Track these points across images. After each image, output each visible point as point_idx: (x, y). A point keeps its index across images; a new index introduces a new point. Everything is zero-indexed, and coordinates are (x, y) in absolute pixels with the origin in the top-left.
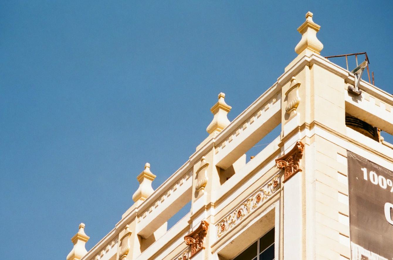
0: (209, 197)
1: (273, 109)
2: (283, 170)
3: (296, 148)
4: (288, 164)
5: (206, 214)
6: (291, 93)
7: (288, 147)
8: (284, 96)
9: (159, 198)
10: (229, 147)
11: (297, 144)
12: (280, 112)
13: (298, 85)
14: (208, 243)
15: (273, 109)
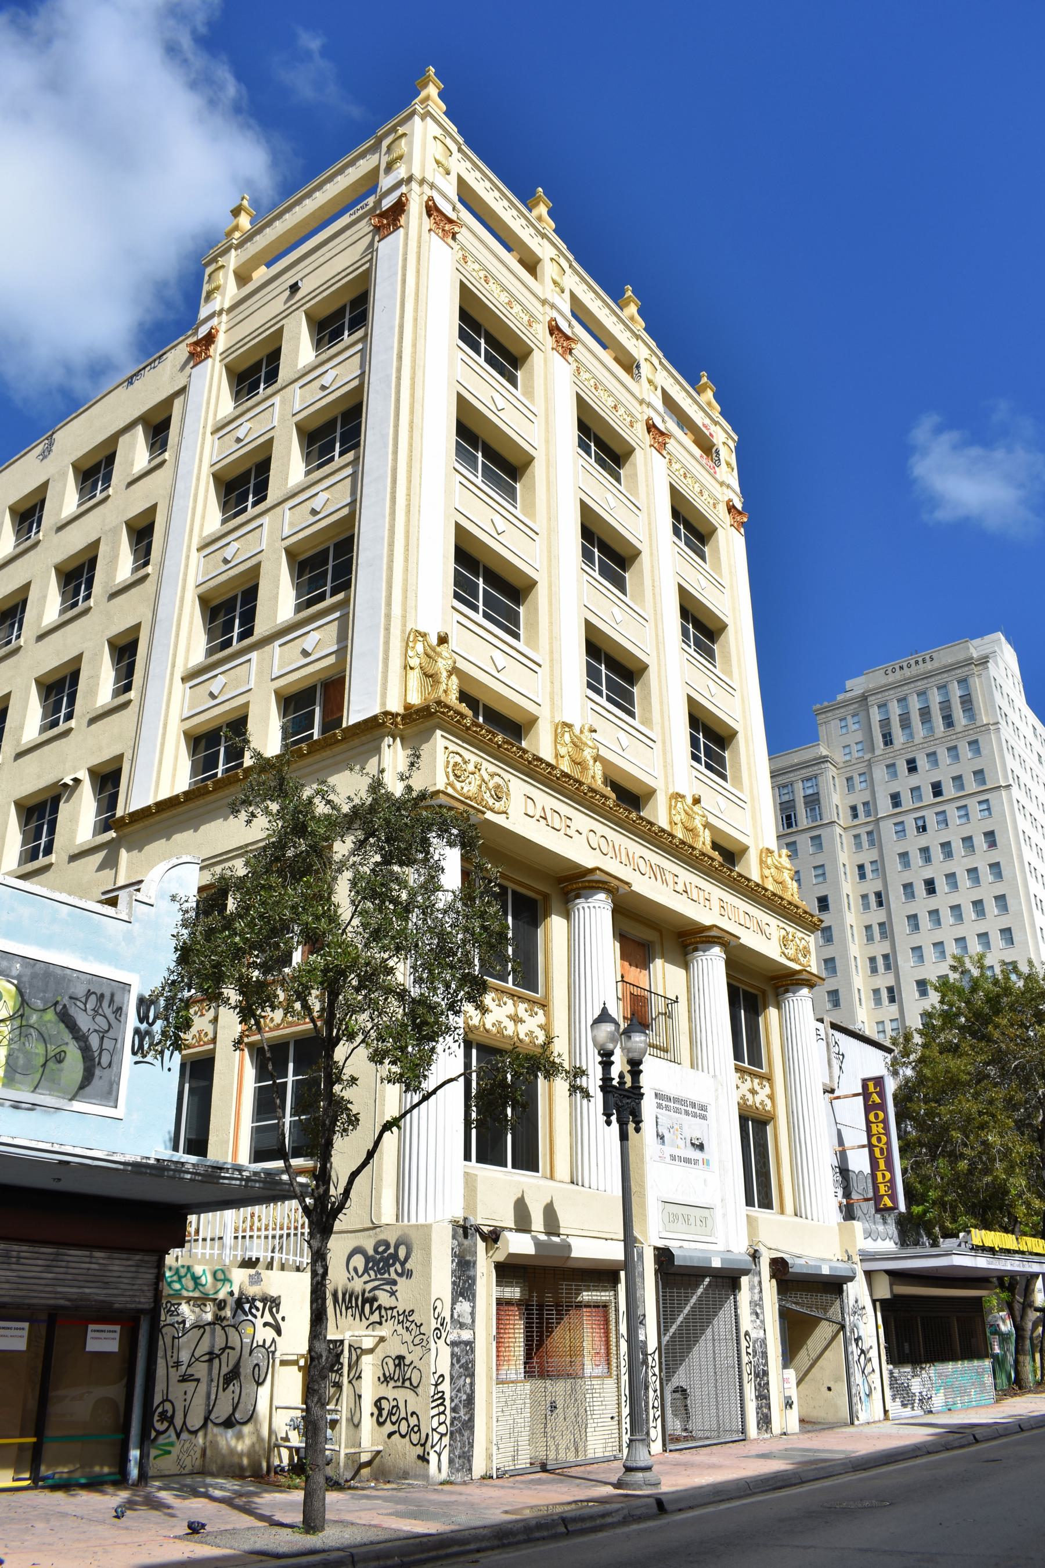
0: (222, 302)
1: (365, 166)
2: (377, 229)
3: (210, 333)
4: (385, 222)
5: (215, 321)
6: (216, 274)
7: (387, 203)
8: (384, 149)
9: (259, 231)
10: (253, 248)
11: (212, 328)
12: (378, 167)
13: (223, 266)
14: (215, 350)
15: (365, 166)
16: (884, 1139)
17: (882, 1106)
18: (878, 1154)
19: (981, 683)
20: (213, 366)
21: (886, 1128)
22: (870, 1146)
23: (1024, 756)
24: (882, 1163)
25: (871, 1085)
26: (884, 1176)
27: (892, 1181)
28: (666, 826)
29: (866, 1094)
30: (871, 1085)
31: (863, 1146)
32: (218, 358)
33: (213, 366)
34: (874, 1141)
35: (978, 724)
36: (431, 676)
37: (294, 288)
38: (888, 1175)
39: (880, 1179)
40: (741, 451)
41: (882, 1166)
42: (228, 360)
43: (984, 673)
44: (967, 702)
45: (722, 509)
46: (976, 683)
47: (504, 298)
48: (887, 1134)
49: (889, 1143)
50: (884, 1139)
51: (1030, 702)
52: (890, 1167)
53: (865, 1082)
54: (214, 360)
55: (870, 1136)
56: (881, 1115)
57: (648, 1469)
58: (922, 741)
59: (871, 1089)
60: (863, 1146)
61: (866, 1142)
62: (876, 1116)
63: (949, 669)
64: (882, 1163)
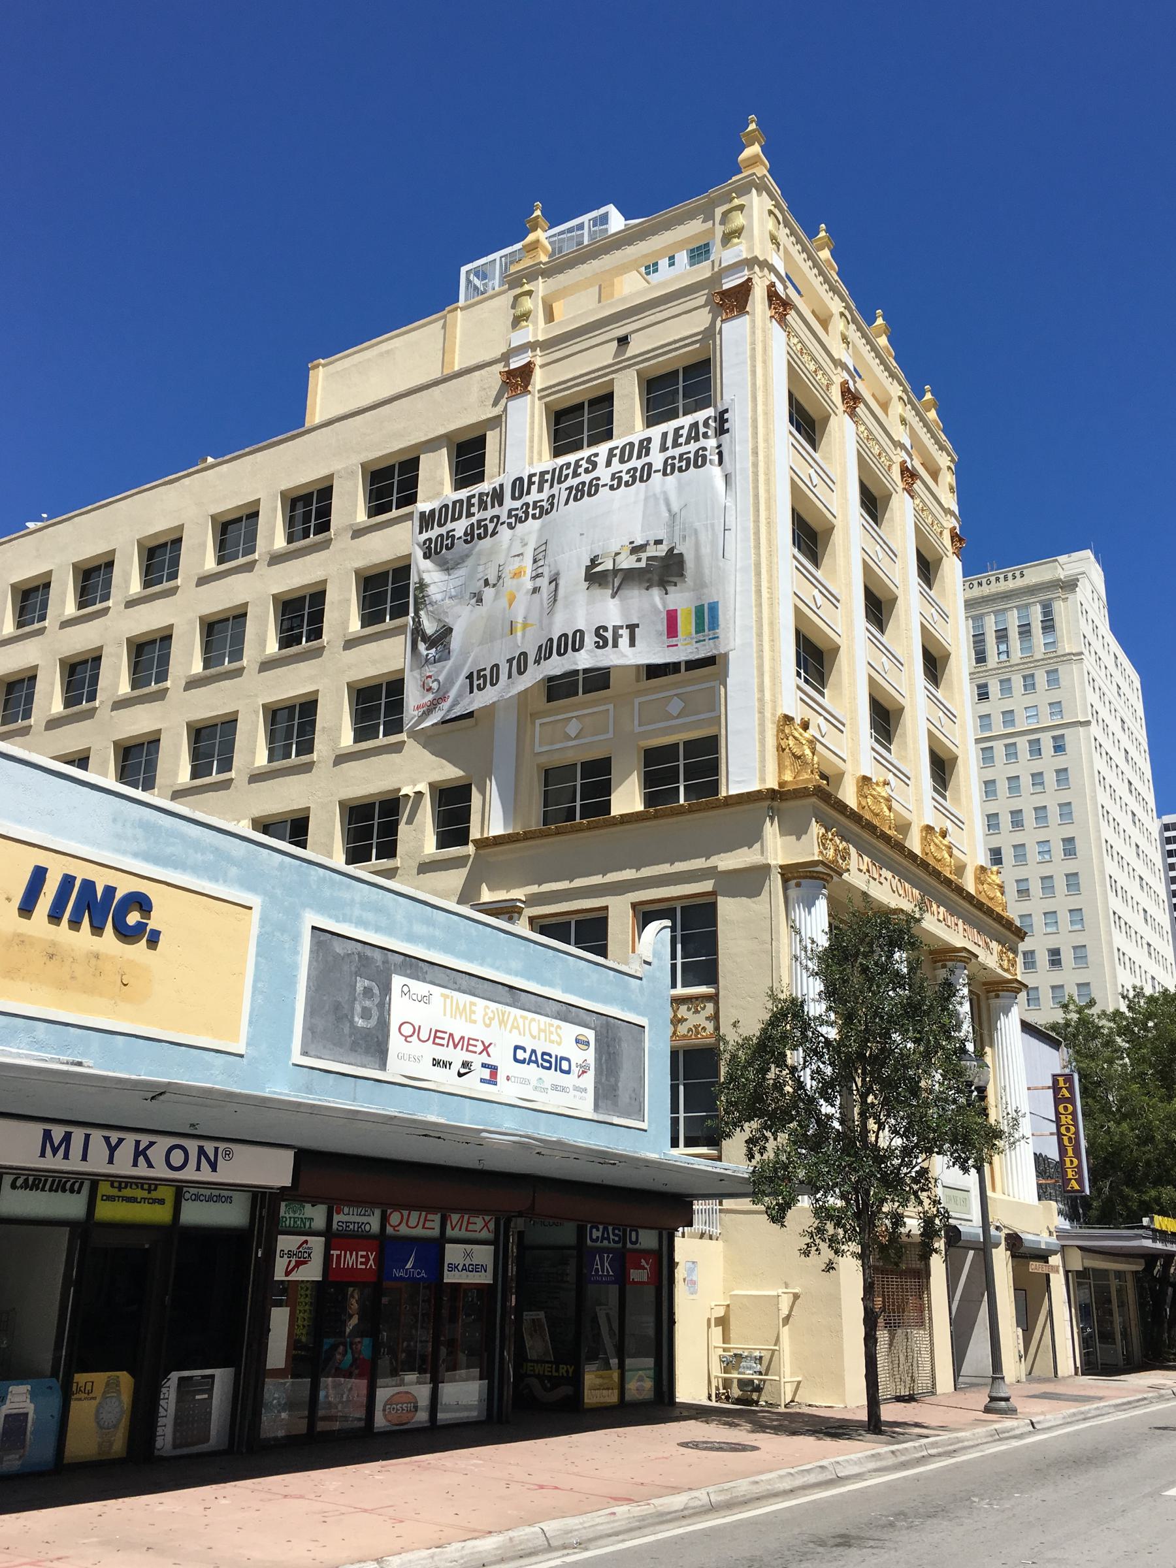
16: (1073, 1129)
17: (1071, 1101)
18: (1066, 1142)
19: (1066, 608)
20: (533, 402)
21: (1075, 1119)
22: (1059, 1135)
23: (1104, 689)
24: (1070, 1150)
25: (1061, 1079)
26: (1072, 1162)
27: (1080, 1166)
28: (973, 892)
29: (1056, 1088)
30: (1061, 1079)
31: (1052, 1134)
32: (537, 395)
33: (533, 402)
34: (1063, 1130)
35: (1060, 653)
36: (799, 758)
37: (623, 341)
38: (1076, 1161)
39: (1068, 1164)
40: (960, 471)
41: (1070, 1153)
42: (548, 399)
43: (1071, 596)
44: (1049, 625)
45: (947, 536)
46: (1059, 607)
47: (812, 367)
48: (1076, 1126)
49: (1077, 1133)
50: (1073, 1129)
51: (1114, 628)
52: (1077, 1153)
53: (1055, 1077)
54: (534, 396)
55: (1058, 1127)
56: (1070, 1108)
57: (1007, 1399)
58: (996, 666)
59: (1061, 1084)
60: (1052, 1134)
61: (1055, 1131)
62: (1066, 1108)
63: (1032, 590)
64: (1070, 1150)
